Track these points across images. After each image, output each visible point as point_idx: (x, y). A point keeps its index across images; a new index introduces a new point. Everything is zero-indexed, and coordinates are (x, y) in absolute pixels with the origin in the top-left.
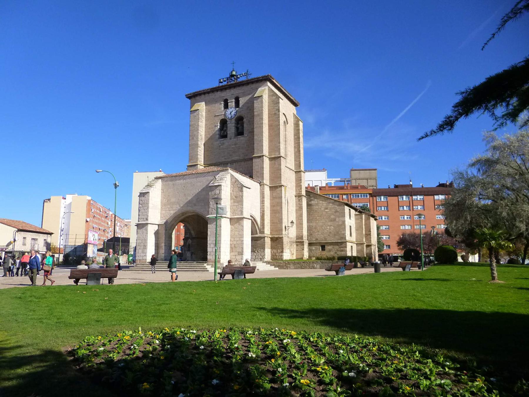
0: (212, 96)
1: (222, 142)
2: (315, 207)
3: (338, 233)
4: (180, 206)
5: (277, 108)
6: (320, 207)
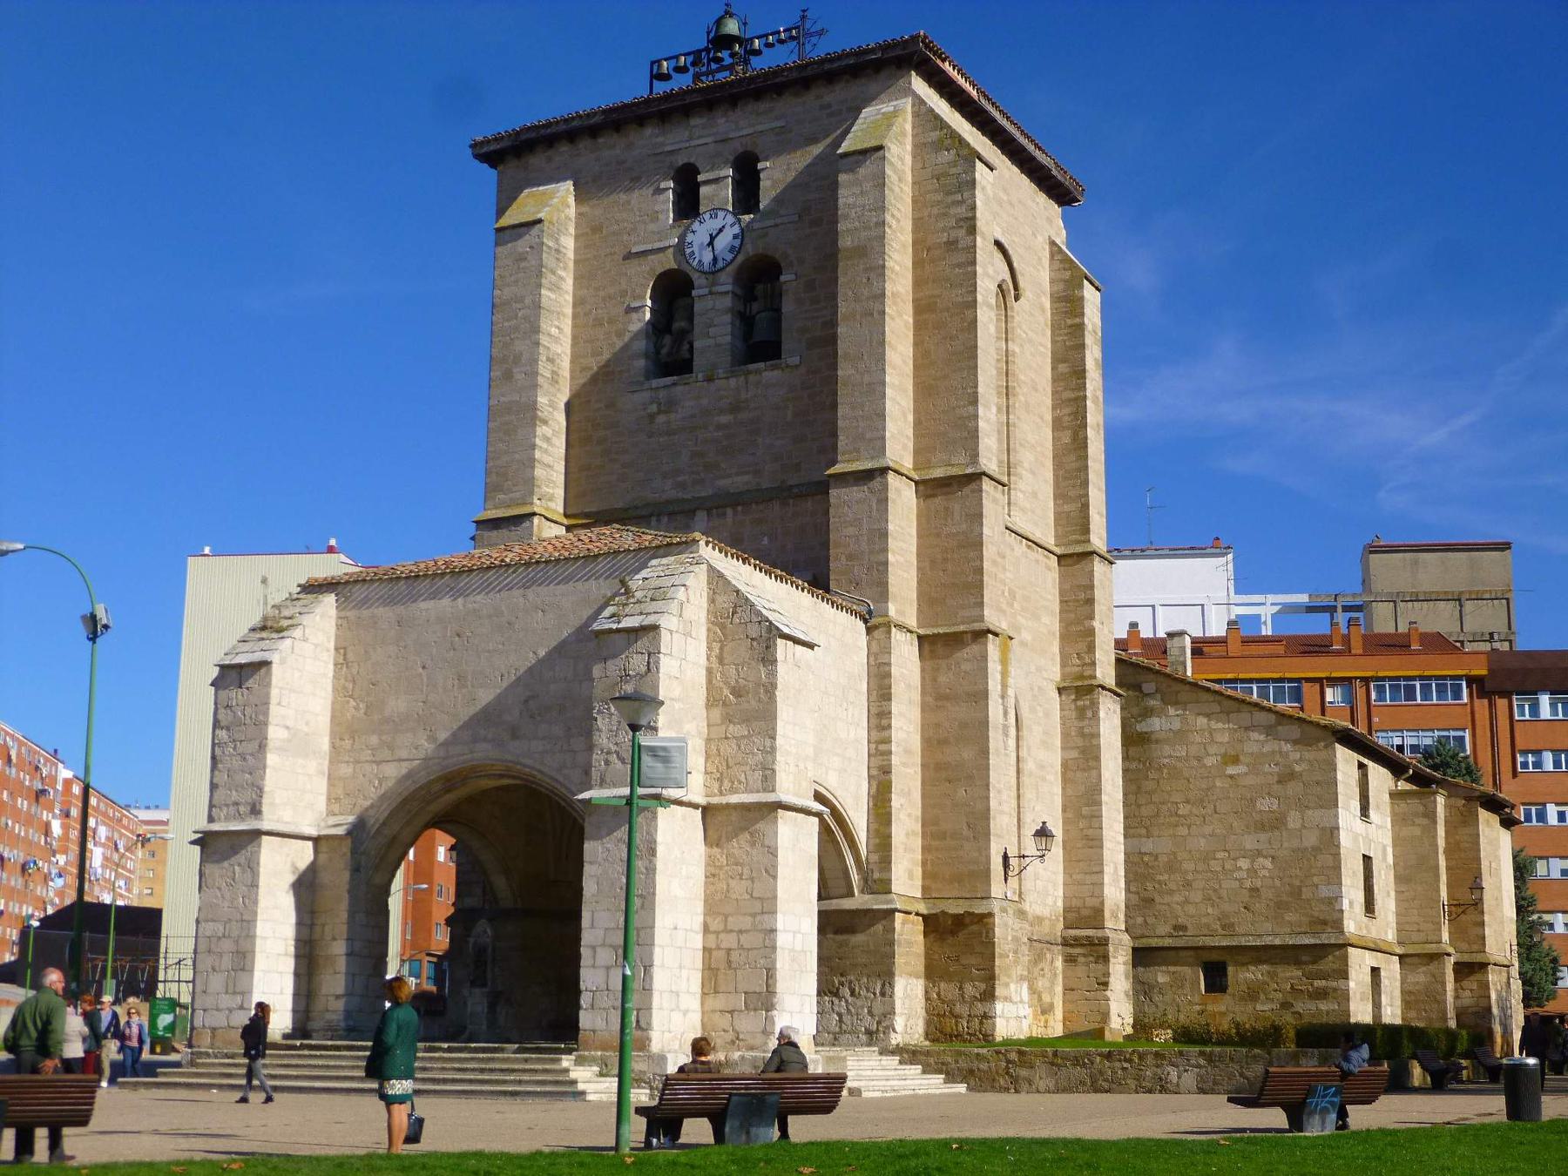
0: (612, 148)
1: (662, 394)
2: (1167, 750)
3: (1296, 893)
4: (431, 739)
5: (961, 211)
6: (1193, 750)
